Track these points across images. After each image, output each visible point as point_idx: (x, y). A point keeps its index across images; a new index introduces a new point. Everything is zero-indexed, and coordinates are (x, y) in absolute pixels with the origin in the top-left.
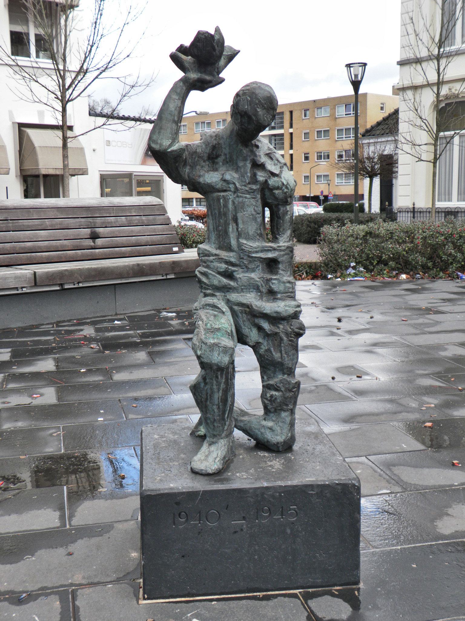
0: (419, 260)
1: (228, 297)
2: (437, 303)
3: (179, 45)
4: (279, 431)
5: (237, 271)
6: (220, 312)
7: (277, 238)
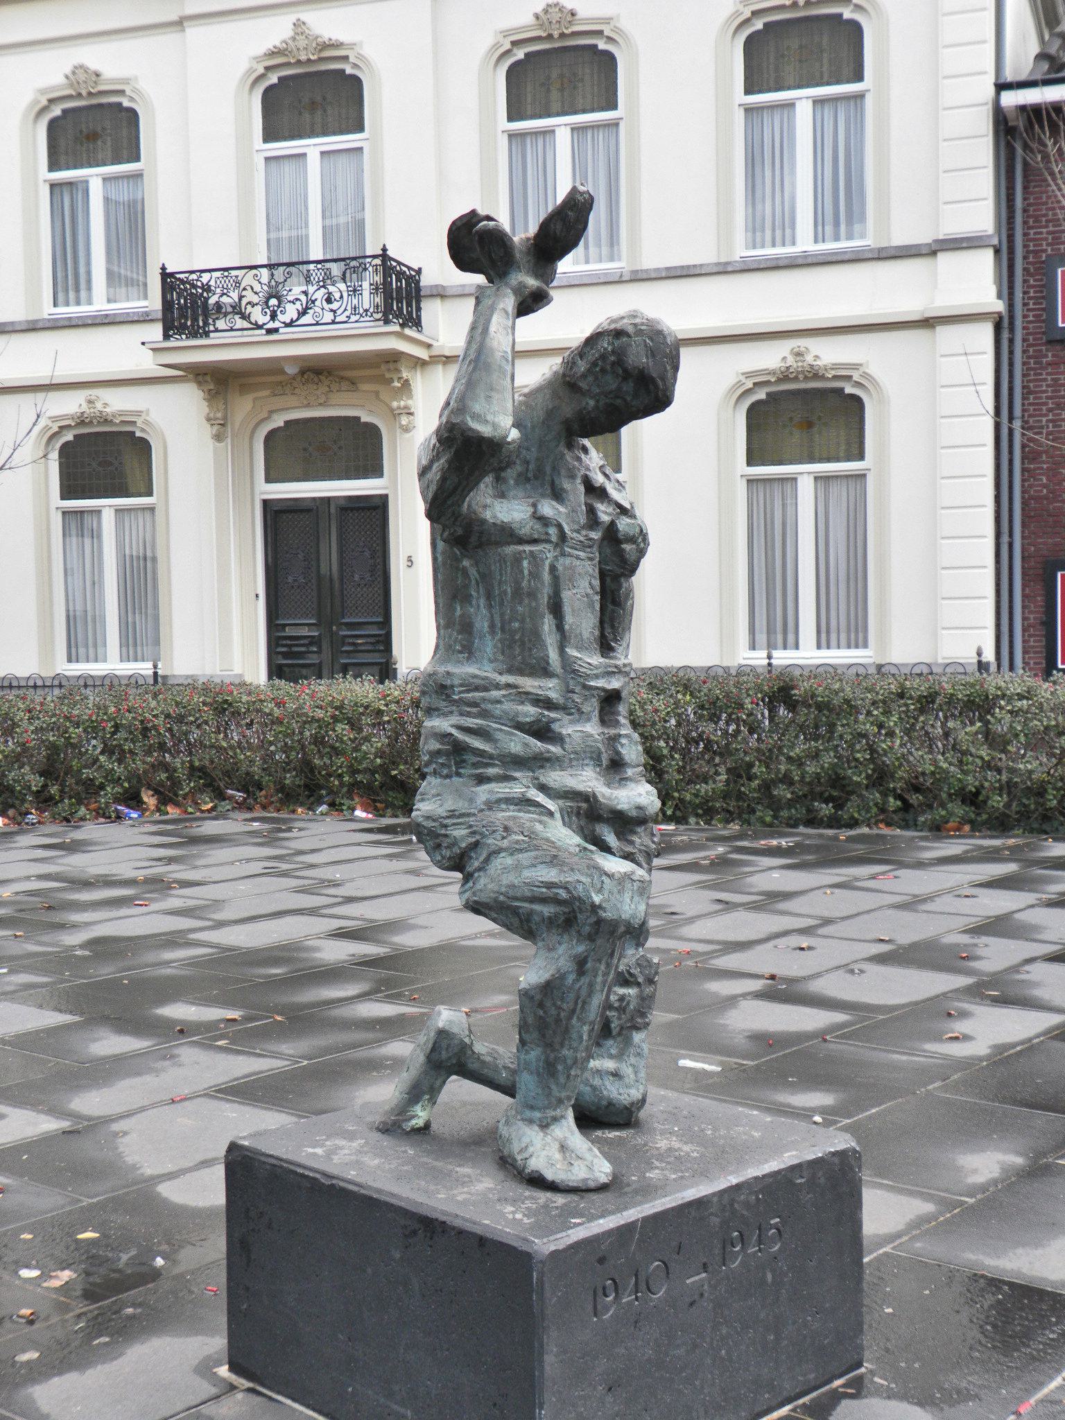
0: (29, 781)
1: (543, 779)
2: (150, 867)
3: (466, 210)
4: (632, 1076)
5: (559, 720)
6: (541, 814)
7: (612, 649)
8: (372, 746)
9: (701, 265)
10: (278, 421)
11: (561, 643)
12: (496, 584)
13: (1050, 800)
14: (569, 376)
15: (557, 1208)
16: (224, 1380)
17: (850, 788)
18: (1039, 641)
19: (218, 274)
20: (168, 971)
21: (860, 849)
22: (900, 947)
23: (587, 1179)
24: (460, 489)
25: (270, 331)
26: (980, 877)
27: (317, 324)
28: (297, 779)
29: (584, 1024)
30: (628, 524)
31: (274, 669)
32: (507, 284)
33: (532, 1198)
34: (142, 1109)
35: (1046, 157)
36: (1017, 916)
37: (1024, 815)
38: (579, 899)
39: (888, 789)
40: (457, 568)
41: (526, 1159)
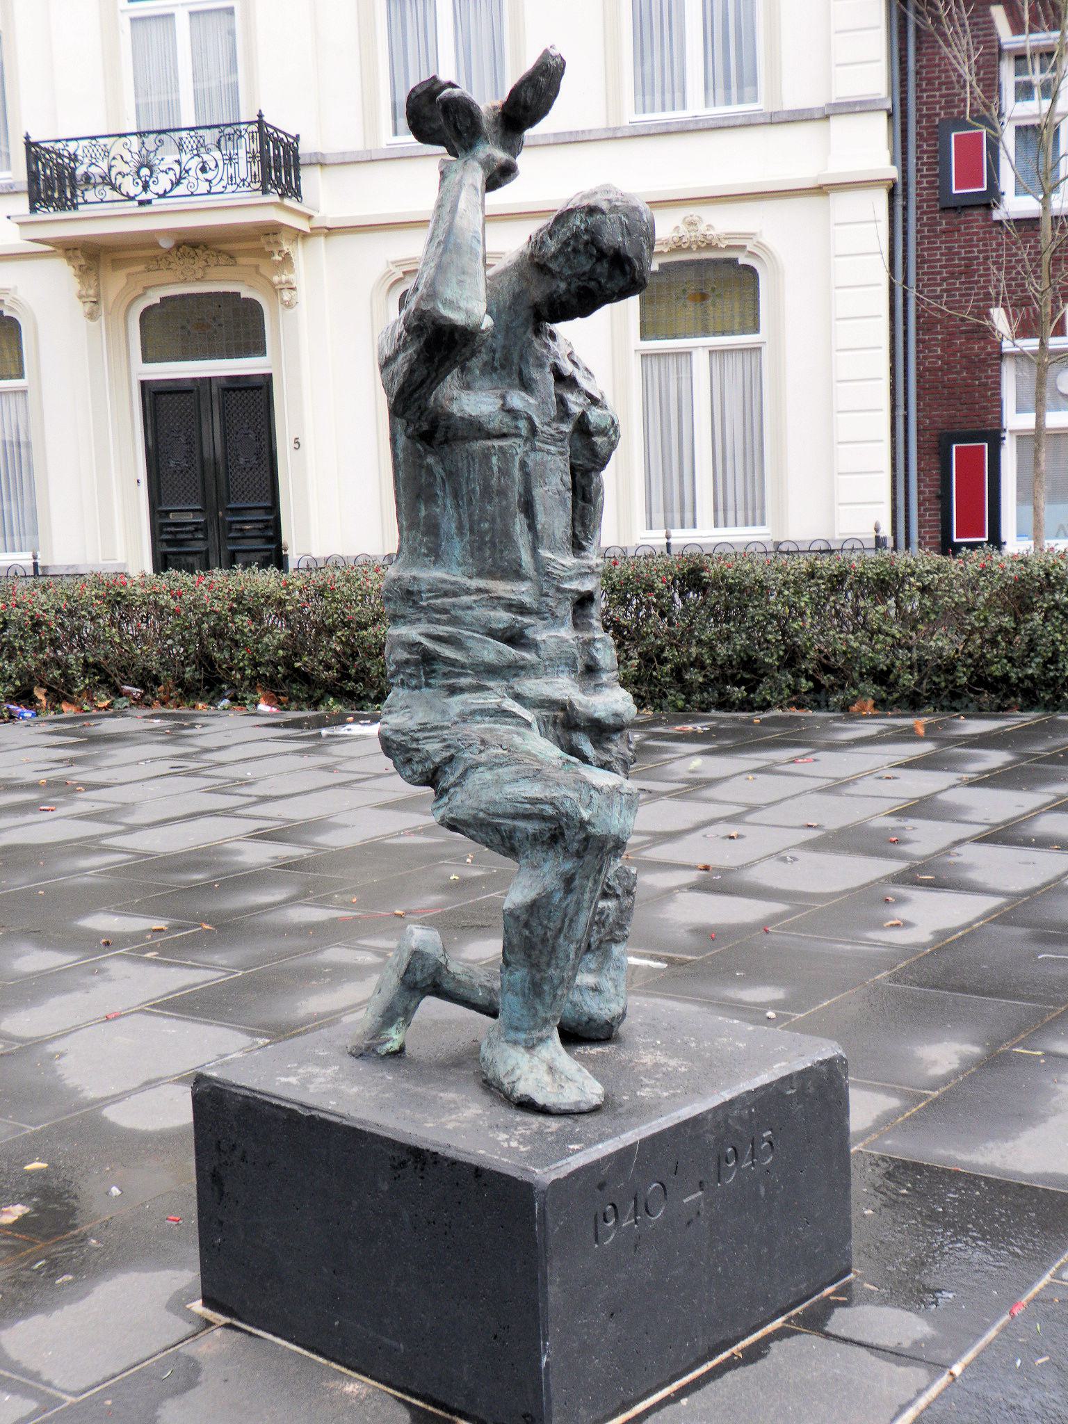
1: (518, 689)
2: (52, 769)
4: (612, 990)
5: (533, 625)
6: (518, 725)
7: (582, 548)
8: (274, 638)
9: (590, 131)
10: (154, 298)
11: (533, 543)
12: (463, 481)
13: (960, 678)
14: (538, 257)
15: (552, 1133)
16: (200, 1317)
17: (761, 672)
18: (935, 515)
19: (86, 142)
20: (85, 880)
21: (776, 733)
22: (829, 832)
23: (580, 1102)
24: (429, 381)
25: (142, 203)
26: (898, 758)
27: (192, 194)
28: (197, 673)
29: (572, 943)
30: (599, 416)
31: (159, 556)
32: (474, 157)
33: (525, 1124)
34: (76, 1029)
35: (937, 19)
36: (940, 797)
37: (935, 692)
38: (567, 815)
39: (799, 670)
40: (421, 466)
41: (514, 1082)
